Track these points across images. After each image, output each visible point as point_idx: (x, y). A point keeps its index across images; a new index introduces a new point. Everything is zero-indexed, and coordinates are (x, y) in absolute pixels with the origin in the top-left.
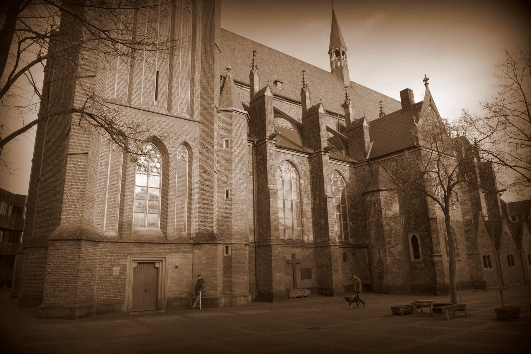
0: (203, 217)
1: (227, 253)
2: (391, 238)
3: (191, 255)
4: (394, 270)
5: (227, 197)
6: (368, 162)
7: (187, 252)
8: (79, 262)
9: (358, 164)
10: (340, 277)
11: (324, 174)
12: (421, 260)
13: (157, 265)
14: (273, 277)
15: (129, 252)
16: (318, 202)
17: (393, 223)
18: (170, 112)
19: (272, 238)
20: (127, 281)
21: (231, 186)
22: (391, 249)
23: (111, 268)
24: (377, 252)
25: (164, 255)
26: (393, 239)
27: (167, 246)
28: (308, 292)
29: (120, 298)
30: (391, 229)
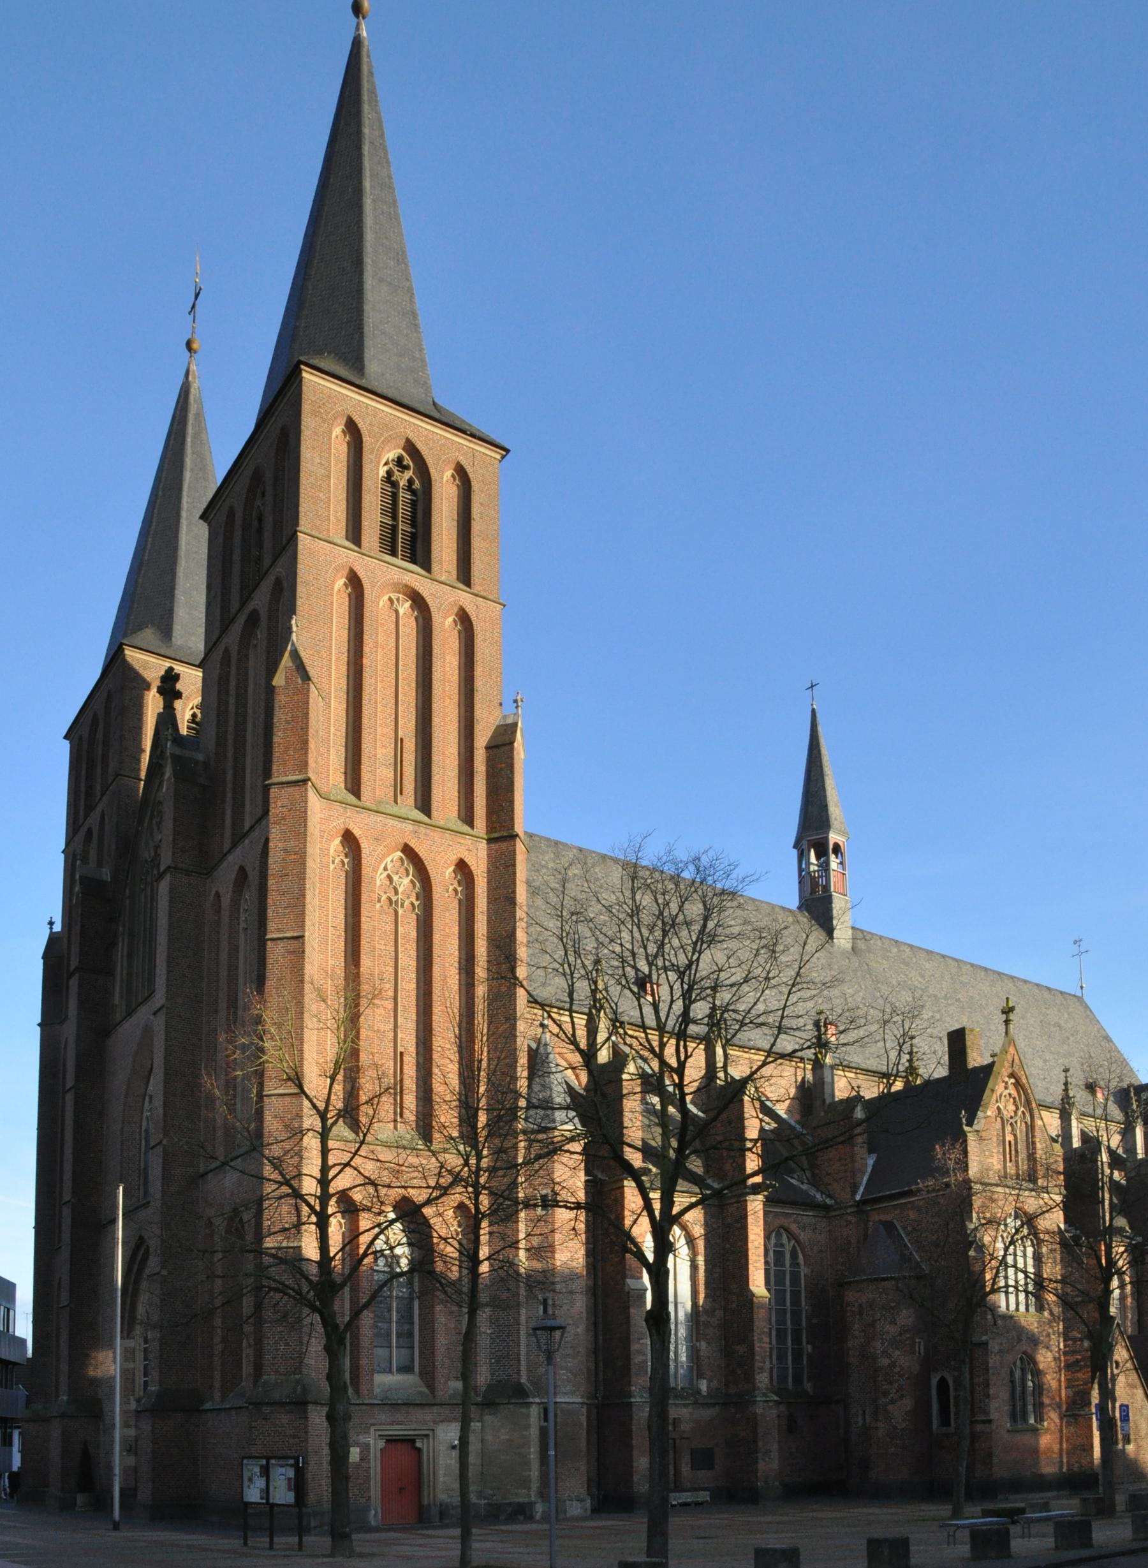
0: (499, 1353)
1: (546, 1419)
2: (891, 1383)
3: (479, 1424)
4: (892, 1450)
5: (545, 1311)
6: (858, 1206)
8: (306, 1441)
9: (835, 1210)
10: (775, 1465)
11: (750, 1245)
12: (952, 1429)
13: (418, 1445)
14: (635, 1464)
15: (372, 1421)
16: (734, 1305)
17: (897, 1353)
19: (633, 1388)
20: (372, 1471)
22: (890, 1407)
24: (861, 1412)
26: (896, 1385)
27: (435, 1409)
28: (704, 1496)
29: (363, 1501)
30: (893, 1365)
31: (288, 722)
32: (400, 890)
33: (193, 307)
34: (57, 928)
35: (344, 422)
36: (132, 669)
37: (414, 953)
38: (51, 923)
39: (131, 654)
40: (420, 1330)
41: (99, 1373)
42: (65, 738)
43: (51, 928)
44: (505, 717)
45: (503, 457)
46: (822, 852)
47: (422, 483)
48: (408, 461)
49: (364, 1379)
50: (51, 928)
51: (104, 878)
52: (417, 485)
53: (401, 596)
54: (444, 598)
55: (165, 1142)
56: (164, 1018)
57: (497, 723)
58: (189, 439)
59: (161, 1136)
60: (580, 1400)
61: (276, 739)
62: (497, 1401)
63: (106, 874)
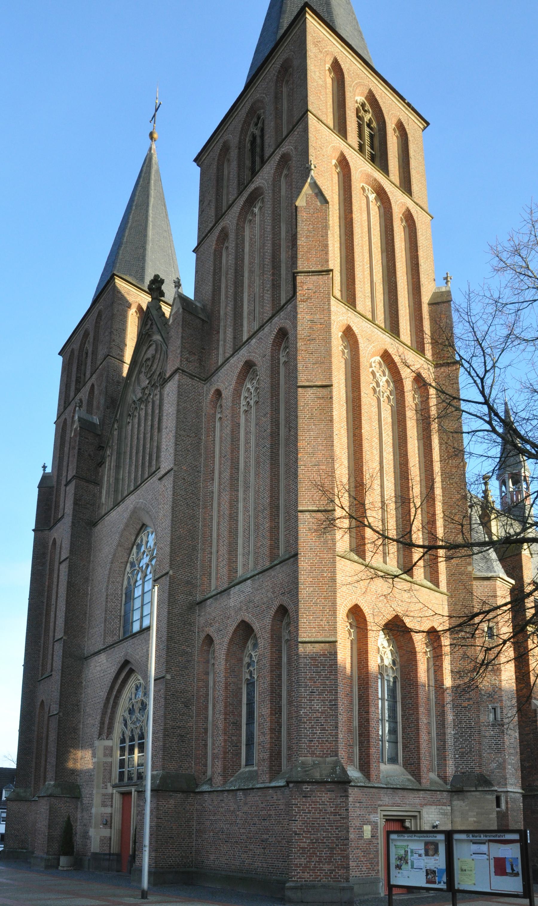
3: (449, 808)
7: (444, 804)
8: (347, 817)
15: (380, 803)
18: (413, 578)
20: (379, 847)
21: (501, 701)
23: (361, 828)
25: (419, 808)
31: (308, 230)
32: (381, 384)
33: (154, 116)
34: (49, 470)
35: (331, 62)
36: (119, 292)
37: (391, 434)
38: (44, 467)
39: (119, 282)
40: (404, 728)
41: (79, 766)
42: (59, 354)
43: (44, 470)
44: (439, 288)
45: (425, 128)
46: (517, 481)
47: (378, 125)
48: (368, 107)
49: (373, 765)
50: (44, 470)
51: (95, 421)
52: (374, 125)
53: (370, 188)
54: (399, 200)
55: (171, 573)
56: (172, 479)
57: (433, 291)
58: (152, 182)
59: (168, 569)
60: (520, 791)
61: (299, 242)
62: (465, 789)
63: (96, 420)
